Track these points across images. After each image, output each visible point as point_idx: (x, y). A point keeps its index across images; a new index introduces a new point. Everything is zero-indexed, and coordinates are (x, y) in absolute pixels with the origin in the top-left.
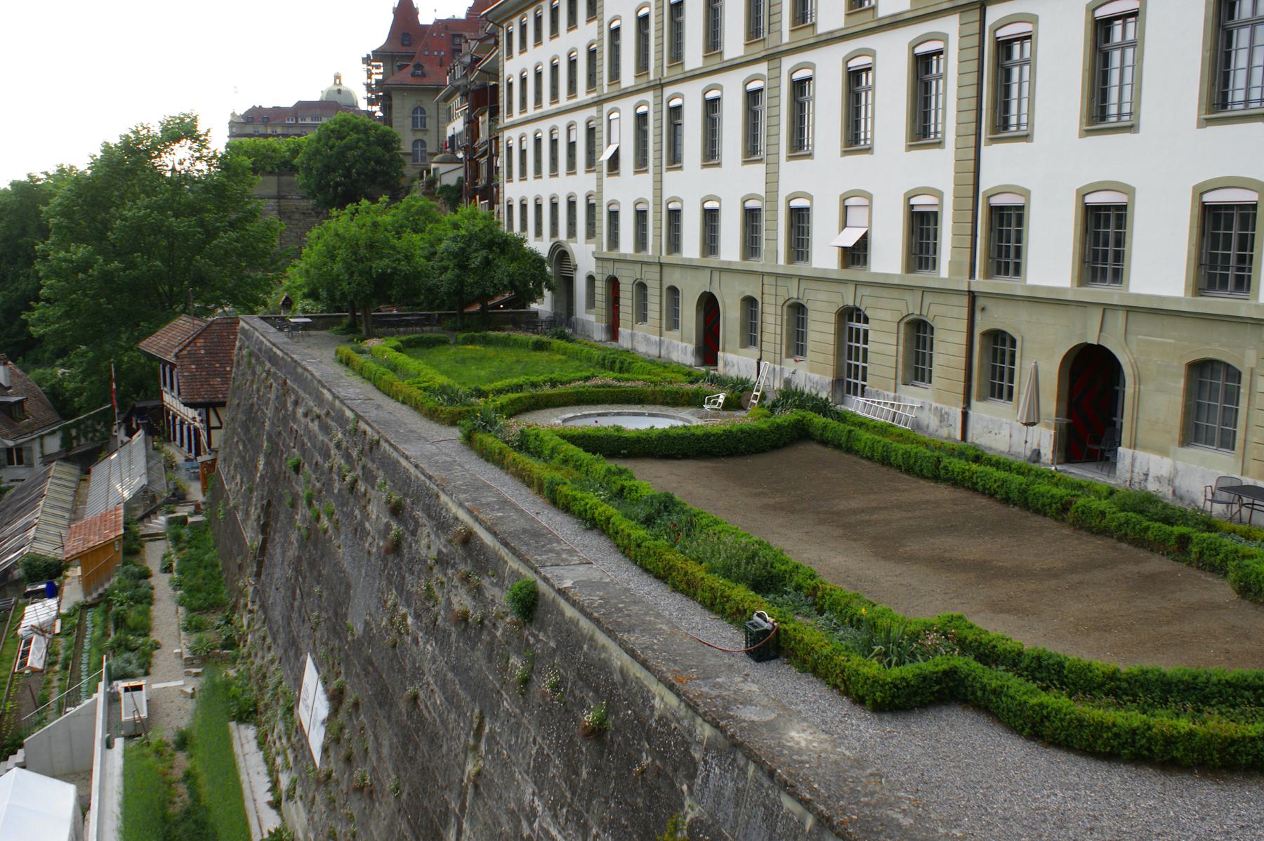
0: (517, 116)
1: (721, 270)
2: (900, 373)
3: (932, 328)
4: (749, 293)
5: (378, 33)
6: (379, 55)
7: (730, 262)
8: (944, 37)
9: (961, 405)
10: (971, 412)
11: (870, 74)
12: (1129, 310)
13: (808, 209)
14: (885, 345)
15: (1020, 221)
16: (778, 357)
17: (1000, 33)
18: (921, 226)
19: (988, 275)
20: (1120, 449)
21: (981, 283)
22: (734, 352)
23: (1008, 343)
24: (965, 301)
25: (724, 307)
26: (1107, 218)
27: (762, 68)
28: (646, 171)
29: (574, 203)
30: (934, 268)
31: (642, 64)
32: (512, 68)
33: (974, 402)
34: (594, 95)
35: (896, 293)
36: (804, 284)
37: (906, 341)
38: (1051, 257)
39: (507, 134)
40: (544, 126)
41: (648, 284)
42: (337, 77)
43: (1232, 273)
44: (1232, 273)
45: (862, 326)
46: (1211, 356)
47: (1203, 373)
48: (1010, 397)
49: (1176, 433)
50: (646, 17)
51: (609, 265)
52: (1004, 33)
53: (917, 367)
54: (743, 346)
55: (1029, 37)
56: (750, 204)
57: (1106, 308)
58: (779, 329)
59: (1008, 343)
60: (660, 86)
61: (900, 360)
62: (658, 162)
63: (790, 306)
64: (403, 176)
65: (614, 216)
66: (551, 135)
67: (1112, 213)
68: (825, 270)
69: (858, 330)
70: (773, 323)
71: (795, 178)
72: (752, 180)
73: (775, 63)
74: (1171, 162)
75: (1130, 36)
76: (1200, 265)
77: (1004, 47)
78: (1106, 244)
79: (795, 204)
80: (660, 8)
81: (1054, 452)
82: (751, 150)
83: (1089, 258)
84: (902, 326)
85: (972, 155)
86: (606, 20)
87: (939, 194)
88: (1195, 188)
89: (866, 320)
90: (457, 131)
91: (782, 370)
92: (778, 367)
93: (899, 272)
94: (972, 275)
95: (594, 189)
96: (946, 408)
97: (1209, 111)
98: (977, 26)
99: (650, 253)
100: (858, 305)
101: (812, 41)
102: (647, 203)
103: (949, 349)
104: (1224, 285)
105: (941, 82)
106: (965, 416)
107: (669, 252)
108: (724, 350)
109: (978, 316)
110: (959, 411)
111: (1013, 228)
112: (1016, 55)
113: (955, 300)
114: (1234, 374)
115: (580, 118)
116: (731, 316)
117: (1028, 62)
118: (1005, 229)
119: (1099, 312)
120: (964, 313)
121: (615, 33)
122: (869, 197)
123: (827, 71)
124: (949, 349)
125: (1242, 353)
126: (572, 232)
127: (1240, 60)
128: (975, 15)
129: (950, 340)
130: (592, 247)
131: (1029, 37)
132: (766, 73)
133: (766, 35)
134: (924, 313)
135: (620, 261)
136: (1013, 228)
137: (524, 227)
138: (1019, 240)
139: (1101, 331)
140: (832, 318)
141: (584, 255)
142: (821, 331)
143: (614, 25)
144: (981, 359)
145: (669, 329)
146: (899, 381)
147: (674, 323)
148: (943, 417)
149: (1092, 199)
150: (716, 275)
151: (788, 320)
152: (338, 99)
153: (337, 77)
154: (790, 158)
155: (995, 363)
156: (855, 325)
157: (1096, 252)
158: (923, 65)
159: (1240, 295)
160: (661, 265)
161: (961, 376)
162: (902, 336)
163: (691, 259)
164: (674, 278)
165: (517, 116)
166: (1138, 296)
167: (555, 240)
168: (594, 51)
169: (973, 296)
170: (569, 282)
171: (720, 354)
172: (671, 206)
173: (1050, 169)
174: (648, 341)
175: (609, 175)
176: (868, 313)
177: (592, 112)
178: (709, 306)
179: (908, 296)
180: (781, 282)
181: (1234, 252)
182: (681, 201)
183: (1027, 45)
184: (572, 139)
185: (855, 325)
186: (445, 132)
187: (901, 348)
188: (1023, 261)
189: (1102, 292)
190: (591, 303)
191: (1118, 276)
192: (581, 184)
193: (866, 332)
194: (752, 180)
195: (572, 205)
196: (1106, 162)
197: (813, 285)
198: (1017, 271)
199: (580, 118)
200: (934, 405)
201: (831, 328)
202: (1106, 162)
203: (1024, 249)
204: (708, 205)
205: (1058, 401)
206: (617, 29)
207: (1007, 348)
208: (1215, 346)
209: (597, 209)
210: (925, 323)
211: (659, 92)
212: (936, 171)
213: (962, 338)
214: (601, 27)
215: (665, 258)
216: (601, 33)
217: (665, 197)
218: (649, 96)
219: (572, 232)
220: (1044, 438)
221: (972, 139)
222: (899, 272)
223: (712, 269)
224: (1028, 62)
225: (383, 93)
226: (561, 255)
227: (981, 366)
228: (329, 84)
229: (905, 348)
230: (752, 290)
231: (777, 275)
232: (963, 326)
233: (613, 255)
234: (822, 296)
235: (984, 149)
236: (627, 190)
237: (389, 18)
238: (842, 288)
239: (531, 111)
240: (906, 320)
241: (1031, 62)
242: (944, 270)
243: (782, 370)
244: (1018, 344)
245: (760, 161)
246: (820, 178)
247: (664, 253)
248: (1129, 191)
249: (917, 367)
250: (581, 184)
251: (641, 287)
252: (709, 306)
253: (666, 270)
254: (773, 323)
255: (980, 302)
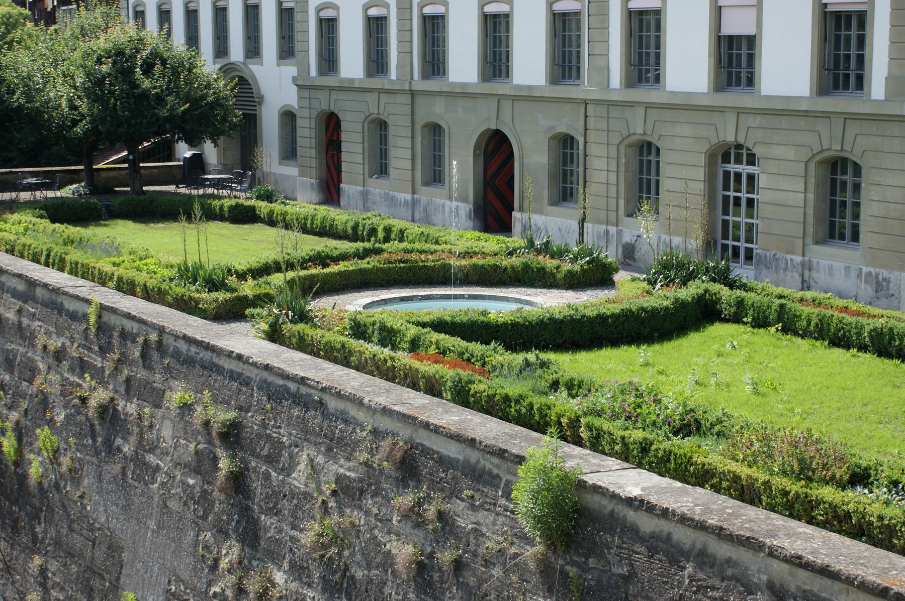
3: (658, 150)
4: (562, 129)
7: (530, 88)
13: (443, 17)
15: (862, 25)
16: (612, 216)
20: (342, 185)
22: (540, 212)
23: (850, 170)
25: (521, 148)
30: (444, 74)
35: (802, 123)
36: (653, 115)
37: (817, 186)
41: (391, 121)
45: (745, 169)
48: (855, 238)
51: (322, 95)
58: (613, 178)
59: (850, 170)
61: (810, 212)
63: (373, 121)
65: (328, 28)
68: (788, 98)
69: (738, 176)
70: (603, 170)
84: (812, 166)
88: (363, 6)
89: (752, 160)
91: (619, 233)
92: (613, 230)
107: (425, 76)
111: (652, 33)
116: (532, 160)
125: (858, 145)
126: (253, 49)
129: (890, 182)
130: (290, 70)
134: (847, 147)
135: (341, 89)
138: (658, 47)
139: (497, 118)
140: (702, 160)
142: (684, 177)
145: (426, 184)
146: (809, 240)
147: (436, 176)
151: (627, 164)
156: (733, 167)
159: (438, 78)
160: (413, 94)
162: (812, 181)
163: (352, 80)
164: (438, 111)
167: (223, 61)
170: (251, 122)
171: (516, 214)
174: (392, 202)
176: (758, 151)
178: (496, 151)
180: (614, 112)
182: (336, 8)
185: (733, 167)
187: (811, 196)
188: (866, 73)
189: (735, 98)
190: (289, 153)
197: (669, 115)
198: (750, 82)
200: (865, 269)
201: (700, 174)
203: (867, 58)
204: (373, 12)
207: (652, 157)
209: (298, 17)
215: (419, 84)
219: (253, 49)
222: (544, 84)
223: (500, 98)
229: (817, 195)
234: (686, 130)
238: (716, 118)
240: (626, 142)
243: (619, 233)
247: (416, 76)
251: (380, 127)
252: (496, 151)
253: (419, 100)
254: (603, 170)
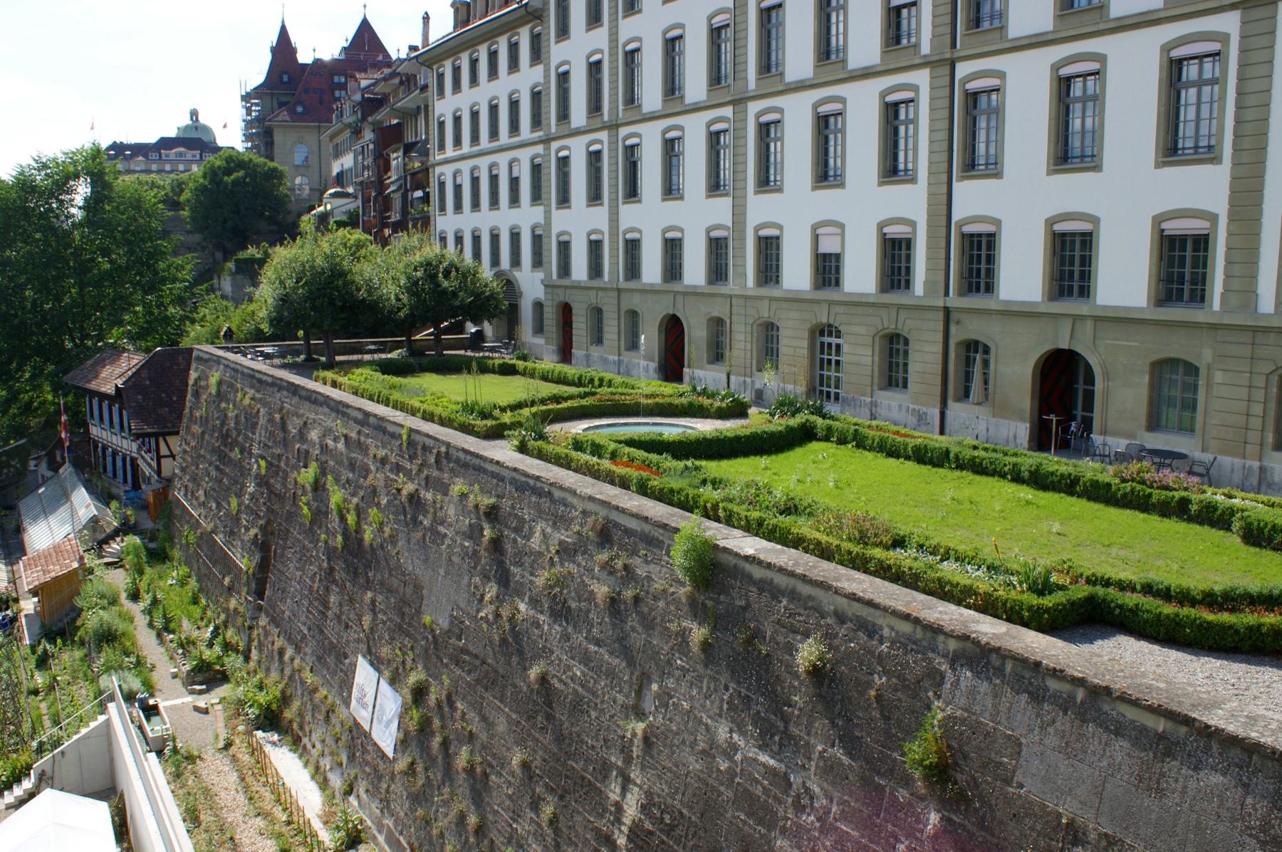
0: (450, 152)
1: (685, 294)
2: (876, 380)
4: (716, 314)
5: (257, 72)
6: (258, 92)
7: (695, 287)
8: (915, 89)
9: (939, 405)
10: (948, 412)
11: (840, 119)
12: (1098, 319)
14: (858, 355)
16: (748, 371)
17: (969, 86)
18: (895, 254)
19: (961, 293)
21: (954, 301)
22: (701, 368)
24: (941, 315)
26: (1073, 242)
27: (728, 111)
28: (601, 204)
29: (518, 234)
31: (595, 106)
32: (444, 107)
33: (950, 403)
34: (541, 133)
35: (871, 310)
37: (881, 351)
38: (1022, 274)
39: (438, 170)
40: (483, 163)
42: (194, 114)
43: (1076, 285)
44: (1076, 285)
45: (834, 340)
46: (1172, 355)
47: (1163, 368)
48: (905, 386)
49: (1143, 420)
50: (599, 63)
51: (560, 291)
52: (973, 86)
53: (893, 374)
54: (711, 362)
55: (912, 101)
56: (715, 234)
57: (1077, 318)
60: (613, 127)
61: (876, 369)
62: (613, 196)
64: (289, 213)
65: (564, 247)
66: (490, 171)
67: (1078, 240)
69: (830, 345)
70: (742, 343)
71: (761, 210)
72: (720, 211)
73: (739, 108)
74: (1131, 197)
75: (1090, 91)
76: (1052, 279)
77: (973, 98)
78: (979, 263)
79: (763, 233)
80: (613, 54)
81: (1030, 442)
82: (595, 196)
83: (966, 274)
84: (877, 339)
85: (945, 190)
86: (554, 62)
87: (913, 224)
88: (1154, 218)
89: (838, 336)
90: (346, 167)
92: (749, 380)
93: (1145, 305)
94: (947, 294)
95: (542, 222)
96: (923, 409)
97: (1056, 164)
98: (947, 79)
99: (1216, 306)
100: (831, 321)
101: (781, 88)
102: (602, 233)
103: (924, 359)
104: (1070, 294)
105: (779, 144)
106: (943, 414)
107: (627, 279)
108: (689, 367)
109: (953, 329)
110: (937, 412)
112: (902, 116)
113: (930, 315)
114: (1192, 370)
115: (525, 155)
117: (912, 121)
118: (978, 256)
119: (1069, 322)
120: (940, 326)
121: (564, 78)
122: (842, 226)
123: (797, 117)
124: (924, 359)
126: (516, 261)
127: (982, 136)
128: (947, 70)
130: (540, 275)
131: (912, 101)
132: (731, 116)
133: (730, 81)
134: (900, 326)
136: (903, 252)
137: (477, 255)
140: (806, 335)
141: (531, 284)
142: (794, 345)
143: (562, 69)
144: (956, 365)
146: (875, 387)
147: (633, 345)
148: (921, 419)
149: (1059, 227)
150: (680, 299)
152: (195, 135)
153: (194, 114)
154: (756, 193)
155: (968, 366)
156: (827, 339)
157: (971, 270)
158: (891, 113)
160: (619, 290)
161: (938, 380)
162: (877, 348)
164: (635, 302)
165: (450, 152)
166: (1105, 307)
168: (539, 93)
169: (947, 311)
170: (514, 309)
171: (686, 370)
172: (629, 236)
173: (1019, 203)
175: (558, 208)
177: (539, 149)
179: (883, 312)
181: (1077, 268)
182: (570, 235)
183: (840, 119)
184: (515, 174)
185: (827, 339)
186: (330, 170)
187: (876, 359)
191: (990, 288)
192: (527, 216)
193: (838, 346)
194: (720, 211)
195: (495, 238)
196: (1074, 194)
198: (837, 283)
199: (525, 155)
200: (911, 407)
202: (1074, 194)
205: (1032, 398)
206: (566, 73)
208: (1176, 347)
210: (772, 324)
211: (614, 132)
212: (910, 203)
213: (939, 348)
214: (547, 71)
215: (623, 284)
216: (547, 76)
217: (622, 227)
218: (604, 135)
220: (1022, 431)
221: (944, 177)
223: (676, 293)
224: (912, 121)
225: (262, 131)
226: (510, 286)
227: (956, 371)
228: (187, 121)
230: (719, 310)
231: (746, 298)
232: (939, 337)
233: (565, 282)
235: (955, 184)
236: (579, 221)
237: (268, 57)
239: (466, 148)
241: (843, 131)
242: (919, 287)
243: (753, 382)
244: (993, 351)
245: (726, 195)
246: (794, 210)
248: (1095, 220)
249: (893, 374)
250: (527, 216)
251: (597, 313)
252: (673, 329)
253: (622, 294)
254: (742, 343)
255: (954, 316)
